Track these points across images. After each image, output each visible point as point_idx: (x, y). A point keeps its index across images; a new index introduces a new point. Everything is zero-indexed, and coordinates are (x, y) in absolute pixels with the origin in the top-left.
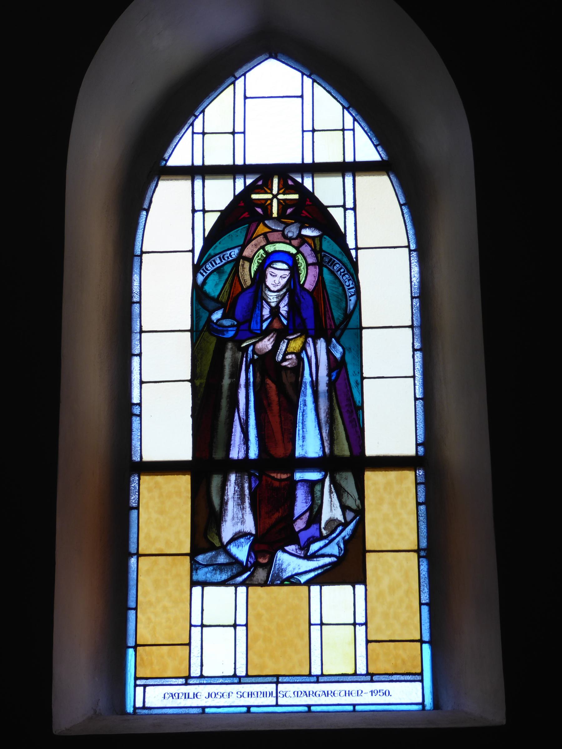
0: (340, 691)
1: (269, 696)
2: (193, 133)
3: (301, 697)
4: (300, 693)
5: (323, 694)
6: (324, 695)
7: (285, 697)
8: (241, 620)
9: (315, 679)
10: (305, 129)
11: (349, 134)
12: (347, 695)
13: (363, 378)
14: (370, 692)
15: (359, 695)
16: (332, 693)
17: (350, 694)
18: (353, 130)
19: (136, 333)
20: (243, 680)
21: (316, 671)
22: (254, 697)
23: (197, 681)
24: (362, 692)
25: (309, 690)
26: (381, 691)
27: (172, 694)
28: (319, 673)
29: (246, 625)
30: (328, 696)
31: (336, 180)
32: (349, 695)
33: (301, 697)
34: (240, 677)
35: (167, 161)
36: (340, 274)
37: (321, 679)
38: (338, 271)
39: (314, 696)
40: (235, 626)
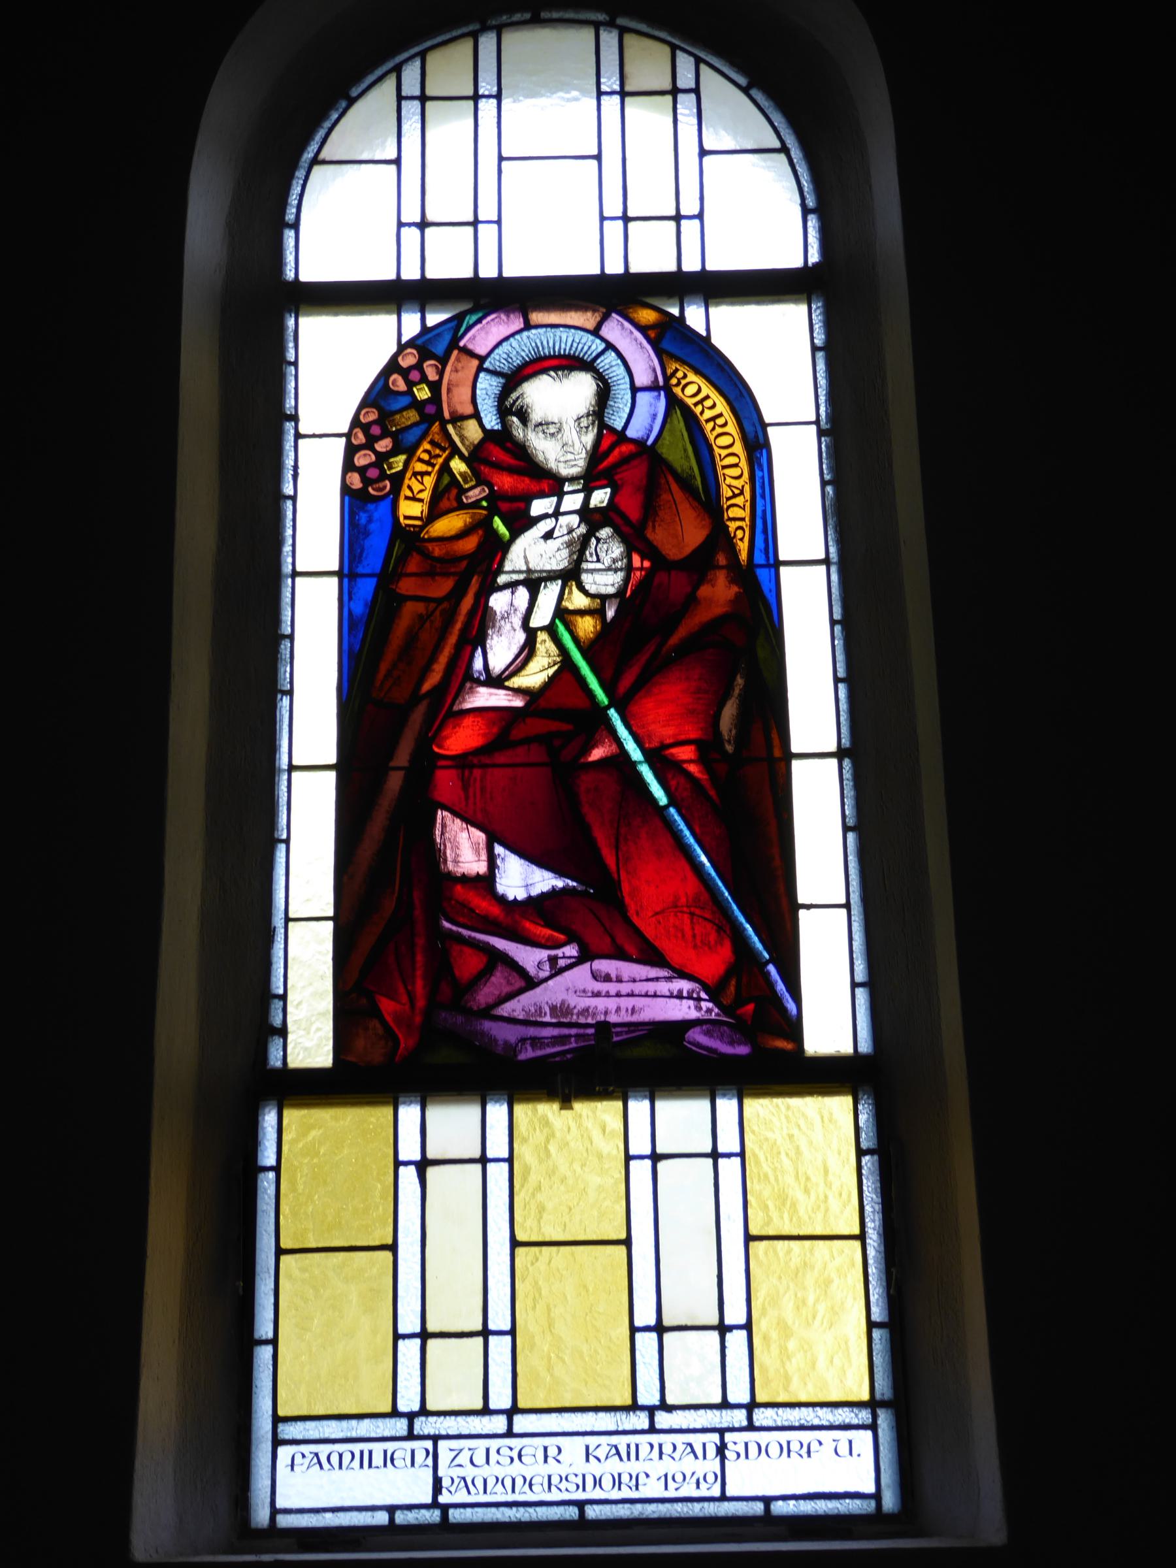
15: (488, 1491)
33: (525, 1493)
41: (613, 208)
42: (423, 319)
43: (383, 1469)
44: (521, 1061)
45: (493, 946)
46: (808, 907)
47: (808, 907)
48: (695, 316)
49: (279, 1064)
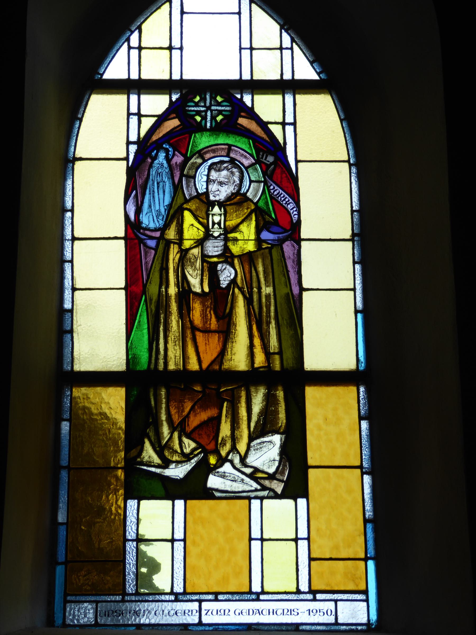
2: (130, 48)
6: (258, 614)
8: (179, 535)
9: (254, 597)
10: (242, 47)
11: (287, 53)
12: (271, 613)
13: (302, 290)
14: (307, 611)
18: (292, 49)
19: (68, 240)
20: (180, 597)
21: (256, 588)
22: (220, 615)
23: (133, 598)
24: (229, 611)
25: (284, 608)
26: (321, 611)
28: (259, 590)
29: (184, 540)
31: (276, 99)
32: (273, 614)
33: (288, 615)
34: (176, 595)
35: (102, 75)
36: (293, 213)
37: (262, 597)
38: (291, 210)
40: (173, 541)
41: (176, 53)
42: (171, 98)
44: (273, 165)
45: (163, 337)
48: (247, 99)
49: (69, 368)
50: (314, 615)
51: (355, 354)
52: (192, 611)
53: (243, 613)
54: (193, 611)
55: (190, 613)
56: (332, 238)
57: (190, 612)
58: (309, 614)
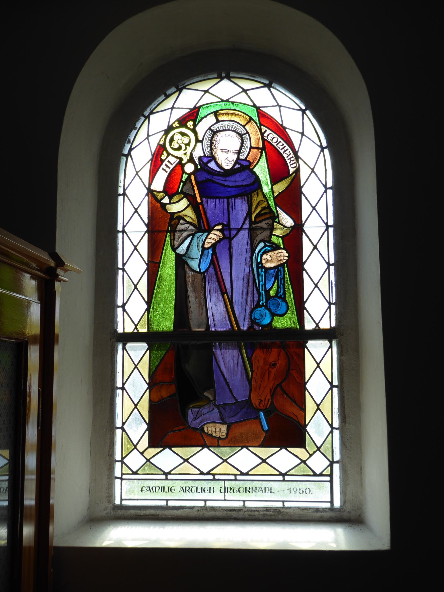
0: (233, 487)
1: (268, 492)
3: (3, 493)
4: (157, 488)
5: (181, 490)
6: (261, 491)
7: (239, 492)
15: (157, 492)
16: (190, 490)
17: (203, 490)
27: (149, 487)
30: (186, 492)
33: (231, 493)
36: (290, 162)
39: (190, 492)
43: (201, 493)
46: (124, 331)
47: (124, 331)
50: (295, 493)
51: (307, 182)
52: (252, 488)
53: (172, 491)
54: (211, 488)
55: (251, 490)
56: (143, 185)
57: (251, 489)
58: (290, 493)
